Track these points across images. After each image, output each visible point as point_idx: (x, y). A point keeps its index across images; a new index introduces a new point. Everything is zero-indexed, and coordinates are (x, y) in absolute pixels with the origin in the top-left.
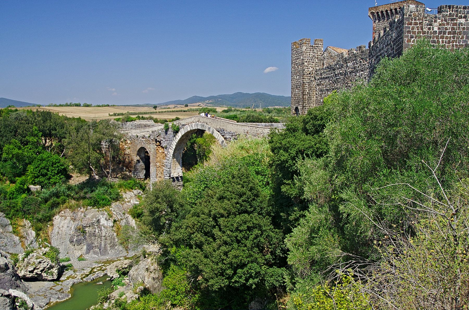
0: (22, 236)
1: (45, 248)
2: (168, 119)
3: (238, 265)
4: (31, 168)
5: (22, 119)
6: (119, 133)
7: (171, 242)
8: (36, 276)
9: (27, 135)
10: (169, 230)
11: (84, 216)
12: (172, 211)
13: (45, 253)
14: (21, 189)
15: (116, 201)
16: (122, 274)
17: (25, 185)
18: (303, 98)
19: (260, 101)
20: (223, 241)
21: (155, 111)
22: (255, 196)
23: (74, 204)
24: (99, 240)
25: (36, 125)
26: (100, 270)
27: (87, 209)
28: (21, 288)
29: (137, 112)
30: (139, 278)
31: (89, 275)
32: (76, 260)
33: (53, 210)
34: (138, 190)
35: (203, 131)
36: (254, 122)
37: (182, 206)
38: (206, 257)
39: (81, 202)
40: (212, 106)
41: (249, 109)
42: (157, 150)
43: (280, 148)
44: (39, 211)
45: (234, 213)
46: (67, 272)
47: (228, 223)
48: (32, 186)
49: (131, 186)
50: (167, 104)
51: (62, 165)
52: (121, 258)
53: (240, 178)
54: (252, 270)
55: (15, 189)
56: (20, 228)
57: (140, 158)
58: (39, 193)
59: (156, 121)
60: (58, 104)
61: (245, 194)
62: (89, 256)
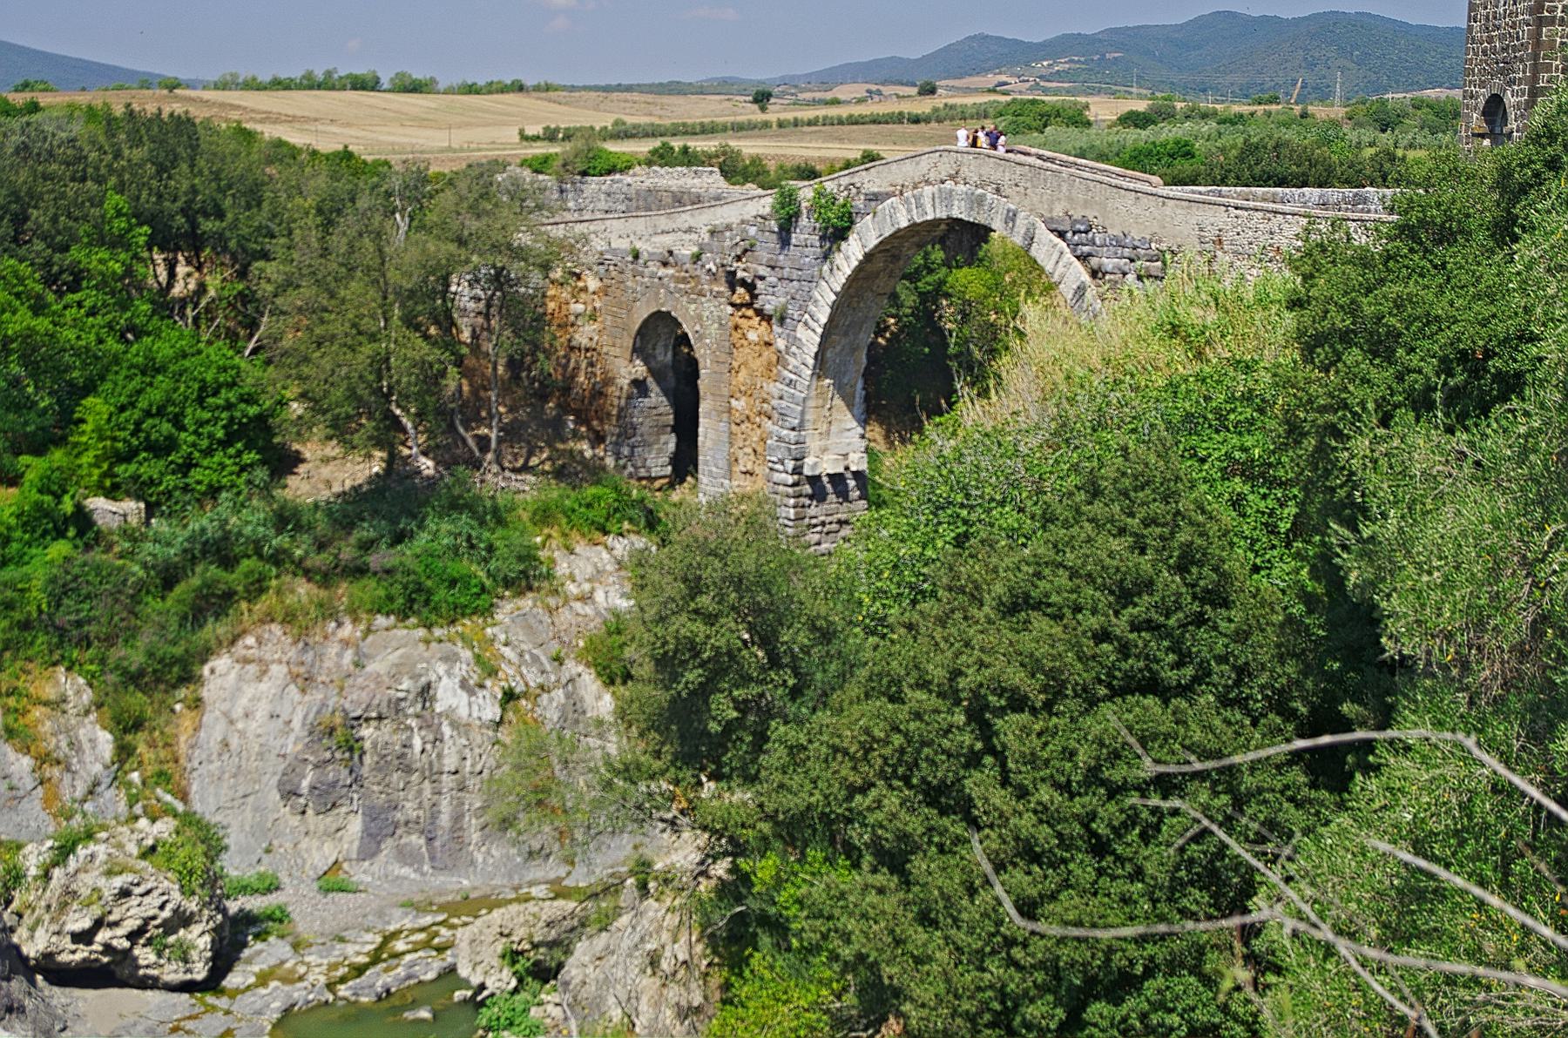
0: (48, 755)
1: (154, 820)
2: (822, 160)
3: (1090, 981)
4: (95, 409)
5: (51, 154)
6: (542, 234)
7: (761, 825)
8: (105, 960)
9: (75, 239)
10: (754, 761)
11: (357, 665)
12: (774, 662)
13: (153, 849)
14: (47, 514)
15: (520, 594)
16: (529, 972)
17: (66, 498)
18: (1538, 44)
19: (1342, 62)
20: (1017, 839)
21: (760, 117)
22: (1203, 601)
23: (305, 599)
24: (427, 793)
25: (120, 188)
26: (427, 945)
27: (368, 631)
28: (31, 1015)
29: (667, 122)
30: (612, 1000)
31: (366, 967)
32: (310, 890)
33: (201, 627)
34: (633, 537)
35: (980, 233)
36: (1282, 183)
37: (826, 635)
38: (926, 919)
39: (344, 590)
40: (1068, 92)
41: (1274, 107)
42: (736, 327)
43: (1346, 337)
44: (133, 632)
45: (1085, 690)
46: (259, 946)
47: (1046, 744)
48: (99, 504)
49: (598, 514)
50: (827, 79)
51: (249, 399)
52: (535, 891)
53: (1126, 496)
54: (1171, 1011)
55: (18, 517)
56: (37, 712)
57: (650, 370)
58: (135, 540)
59: (735, 170)
60: (265, 77)
61: (1148, 585)
62: (375, 868)
